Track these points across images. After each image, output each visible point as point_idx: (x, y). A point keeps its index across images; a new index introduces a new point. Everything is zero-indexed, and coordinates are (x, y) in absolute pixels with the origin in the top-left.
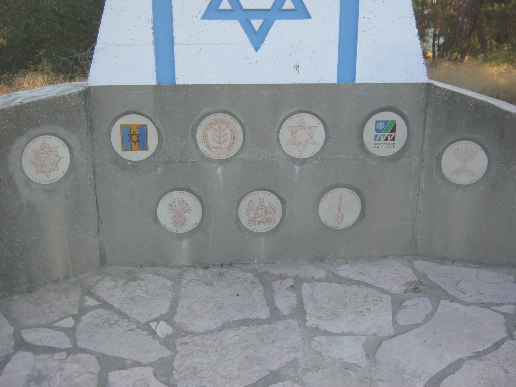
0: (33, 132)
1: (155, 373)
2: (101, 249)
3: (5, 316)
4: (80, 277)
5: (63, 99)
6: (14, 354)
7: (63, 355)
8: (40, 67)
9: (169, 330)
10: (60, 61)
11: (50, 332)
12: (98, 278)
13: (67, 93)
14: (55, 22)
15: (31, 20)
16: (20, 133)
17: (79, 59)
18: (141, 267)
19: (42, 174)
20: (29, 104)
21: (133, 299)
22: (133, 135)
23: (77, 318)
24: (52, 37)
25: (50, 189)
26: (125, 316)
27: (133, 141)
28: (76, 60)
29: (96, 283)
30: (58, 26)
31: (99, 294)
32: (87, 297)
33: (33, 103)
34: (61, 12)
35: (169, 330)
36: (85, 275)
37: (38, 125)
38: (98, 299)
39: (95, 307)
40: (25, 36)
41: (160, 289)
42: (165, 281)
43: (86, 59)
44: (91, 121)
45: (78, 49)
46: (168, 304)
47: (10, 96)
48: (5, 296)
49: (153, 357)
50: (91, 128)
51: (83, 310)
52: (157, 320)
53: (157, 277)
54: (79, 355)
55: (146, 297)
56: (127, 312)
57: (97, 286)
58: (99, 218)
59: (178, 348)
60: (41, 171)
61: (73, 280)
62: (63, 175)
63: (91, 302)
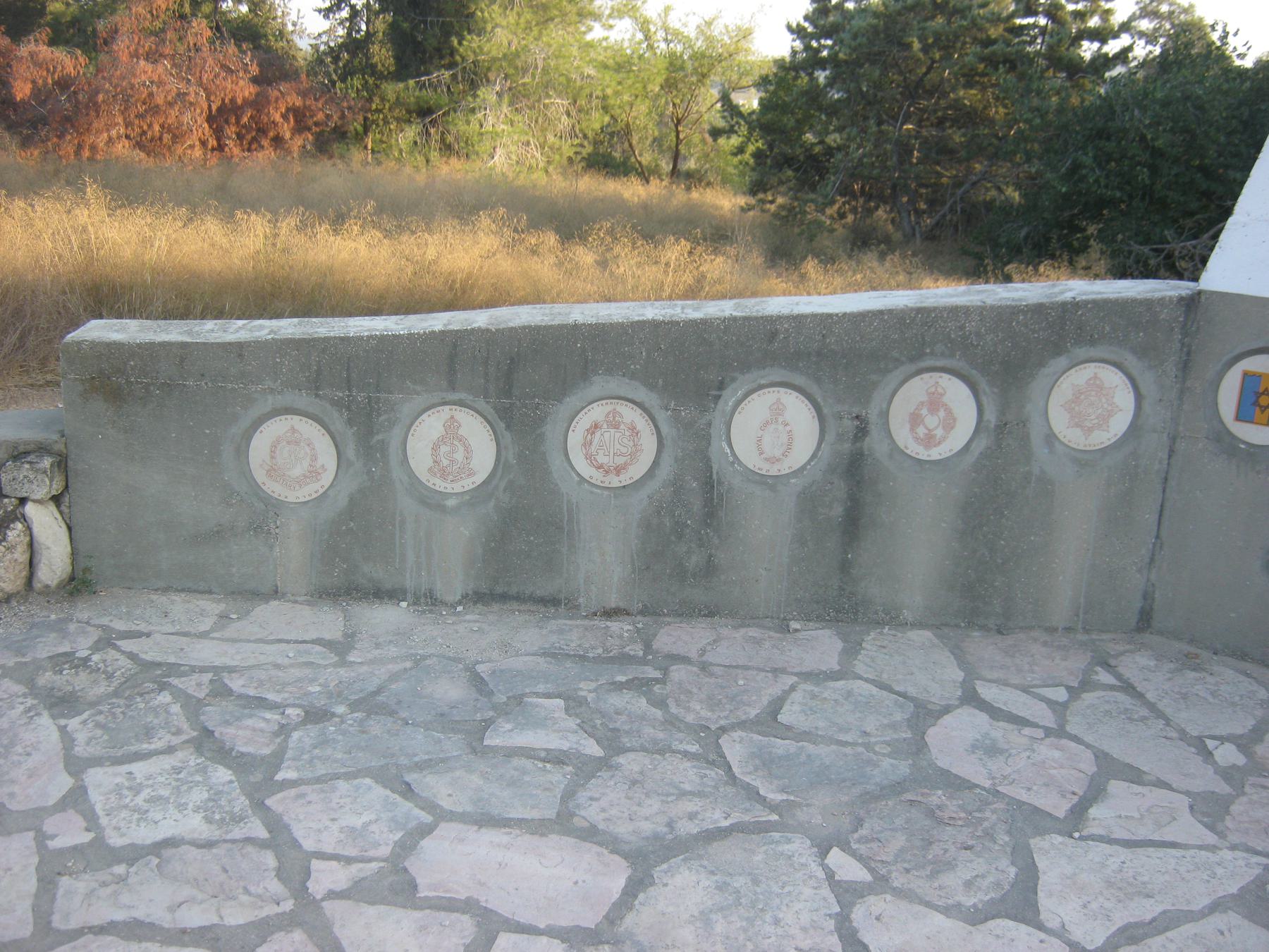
0: (1081, 352)
1: (1191, 807)
2: (1147, 596)
3: (953, 653)
4: (1094, 637)
5: (1148, 304)
6: (957, 707)
7: (1040, 733)
8: (1082, 261)
9: (1241, 760)
10: (1130, 252)
11: (1024, 697)
12: (1128, 647)
13: (1157, 295)
14: (1139, 163)
15: (1086, 154)
16: (1058, 349)
17: (1177, 253)
18: (1215, 653)
19: (1078, 431)
20: (1086, 302)
21: (1185, 697)
22: (1263, 394)
23: (1074, 693)
24: (1125, 198)
25: (1084, 461)
26: (1160, 715)
27: (1261, 407)
28: (1170, 256)
29: (1122, 654)
30: (1143, 175)
31: (1121, 670)
32: (1099, 669)
33: (1094, 302)
34: (1159, 143)
35: (1241, 760)
36: (1104, 636)
37: (1092, 342)
38: (1119, 677)
39: (1112, 688)
40: (1064, 190)
41: (1241, 696)
42: (1255, 687)
43: (1192, 258)
44: (1188, 354)
45: (1180, 232)
46: (1250, 723)
47: (1054, 286)
48: (958, 626)
49: (1198, 785)
50: (1185, 367)
51: (1086, 685)
52: (1222, 739)
53: (1242, 678)
54: (1064, 742)
55: (1211, 700)
56: (1169, 711)
57: (1123, 658)
58: (1157, 537)
59: (1247, 789)
60: (1077, 425)
61: (1081, 637)
62: (1113, 440)
63: (1104, 677)
